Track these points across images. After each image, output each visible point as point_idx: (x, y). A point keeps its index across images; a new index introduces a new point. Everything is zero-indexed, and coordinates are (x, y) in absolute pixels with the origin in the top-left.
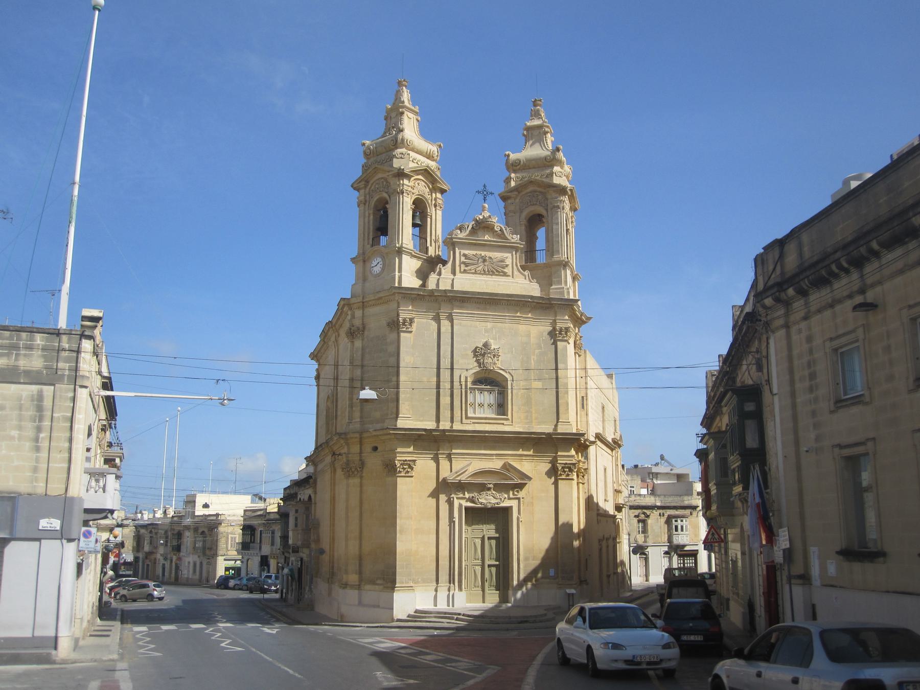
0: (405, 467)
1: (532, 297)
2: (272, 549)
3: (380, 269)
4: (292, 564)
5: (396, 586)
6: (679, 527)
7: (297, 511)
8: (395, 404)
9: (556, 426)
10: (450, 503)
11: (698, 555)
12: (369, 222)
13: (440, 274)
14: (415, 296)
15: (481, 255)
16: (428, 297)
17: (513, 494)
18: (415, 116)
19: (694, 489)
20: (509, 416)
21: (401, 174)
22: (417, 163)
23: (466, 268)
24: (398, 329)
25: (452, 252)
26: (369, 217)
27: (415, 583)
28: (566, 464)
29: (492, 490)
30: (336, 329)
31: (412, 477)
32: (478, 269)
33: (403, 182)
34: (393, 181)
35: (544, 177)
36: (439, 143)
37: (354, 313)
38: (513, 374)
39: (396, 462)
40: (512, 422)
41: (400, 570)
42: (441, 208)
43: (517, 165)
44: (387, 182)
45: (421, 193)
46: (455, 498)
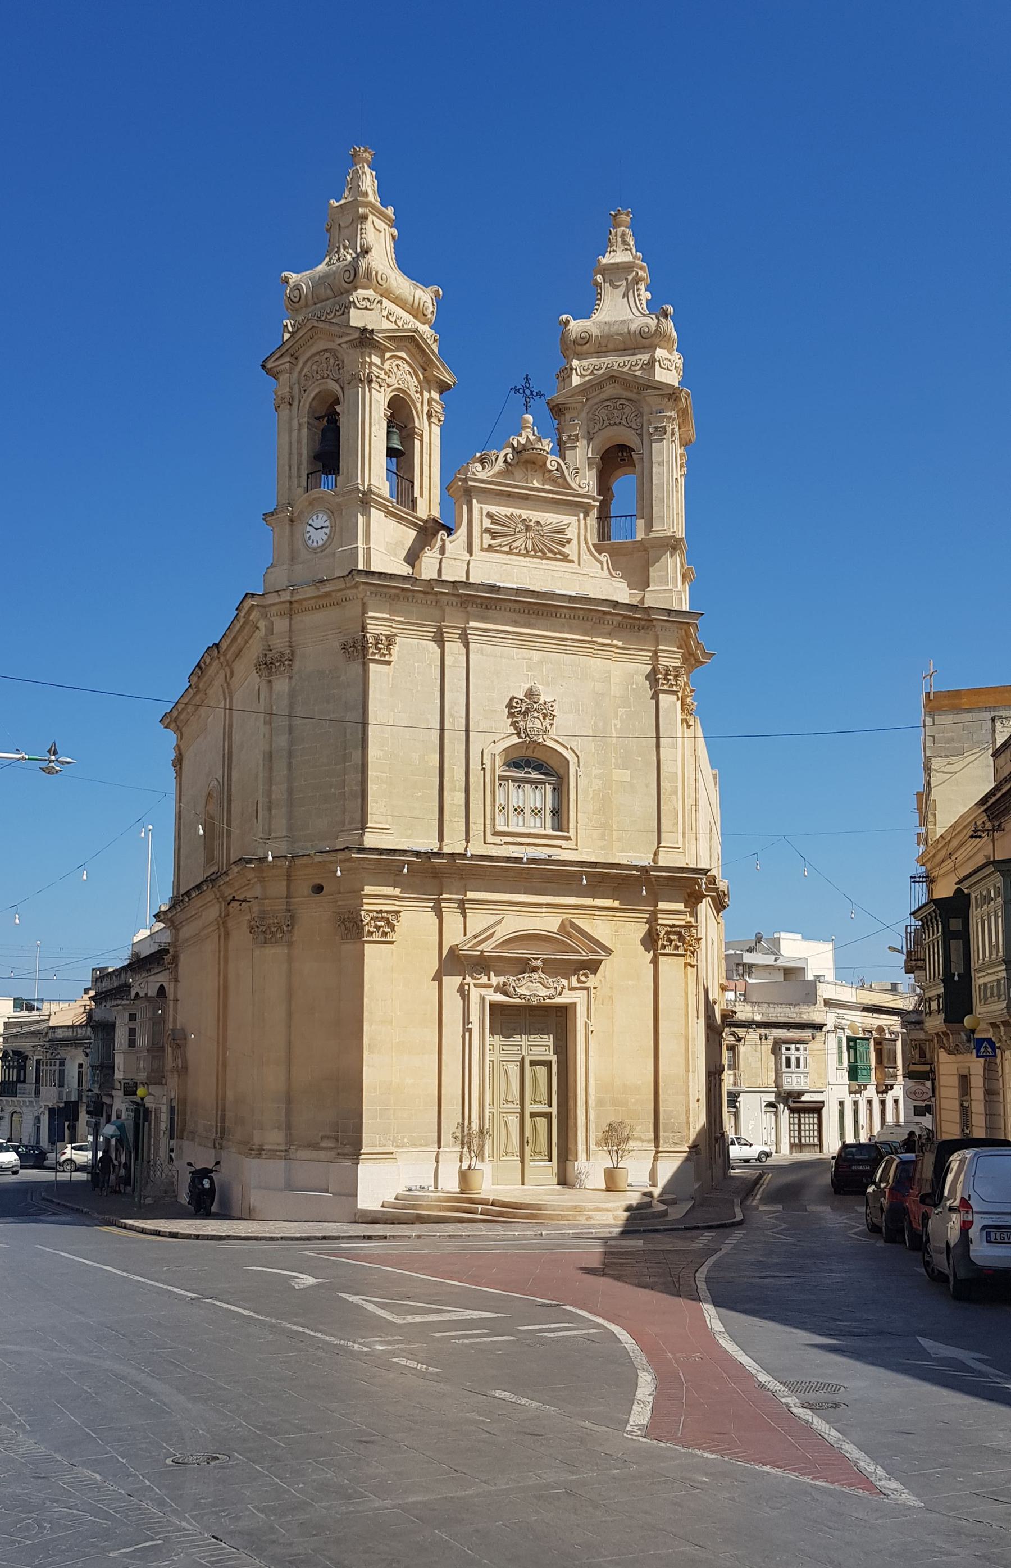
0: (379, 924)
1: (616, 604)
2: (60, 1094)
3: (325, 537)
4: (119, 1117)
5: (362, 1151)
6: (793, 1061)
7: (132, 1017)
8: (359, 800)
9: (656, 854)
10: (463, 992)
11: (824, 1110)
12: (299, 442)
13: (442, 550)
14: (397, 591)
15: (520, 517)
16: (421, 595)
17: (579, 981)
18: (387, 227)
19: (819, 993)
20: (572, 833)
21: (365, 339)
22: (395, 322)
23: (493, 542)
24: (364, 657)
25: (465, 507)
26: (299, 430)
27: (397, 1146)
28: (674, 926)
29: (540, 972)
30: (227, 661)
31: (392, 943)
32: (514, 545)
33: (371, 359)
34: (349, 355)
35: (638, 368)
36: (435, 288)
37: (272, 623)
38: (578, 753)
39: (363, 913)
40: (576, 845)
41: (370, 1121)
42: (439, 421)
43: (586, 340)
44: (337, 359)
45: (402, 386)
46: (472, 986)
